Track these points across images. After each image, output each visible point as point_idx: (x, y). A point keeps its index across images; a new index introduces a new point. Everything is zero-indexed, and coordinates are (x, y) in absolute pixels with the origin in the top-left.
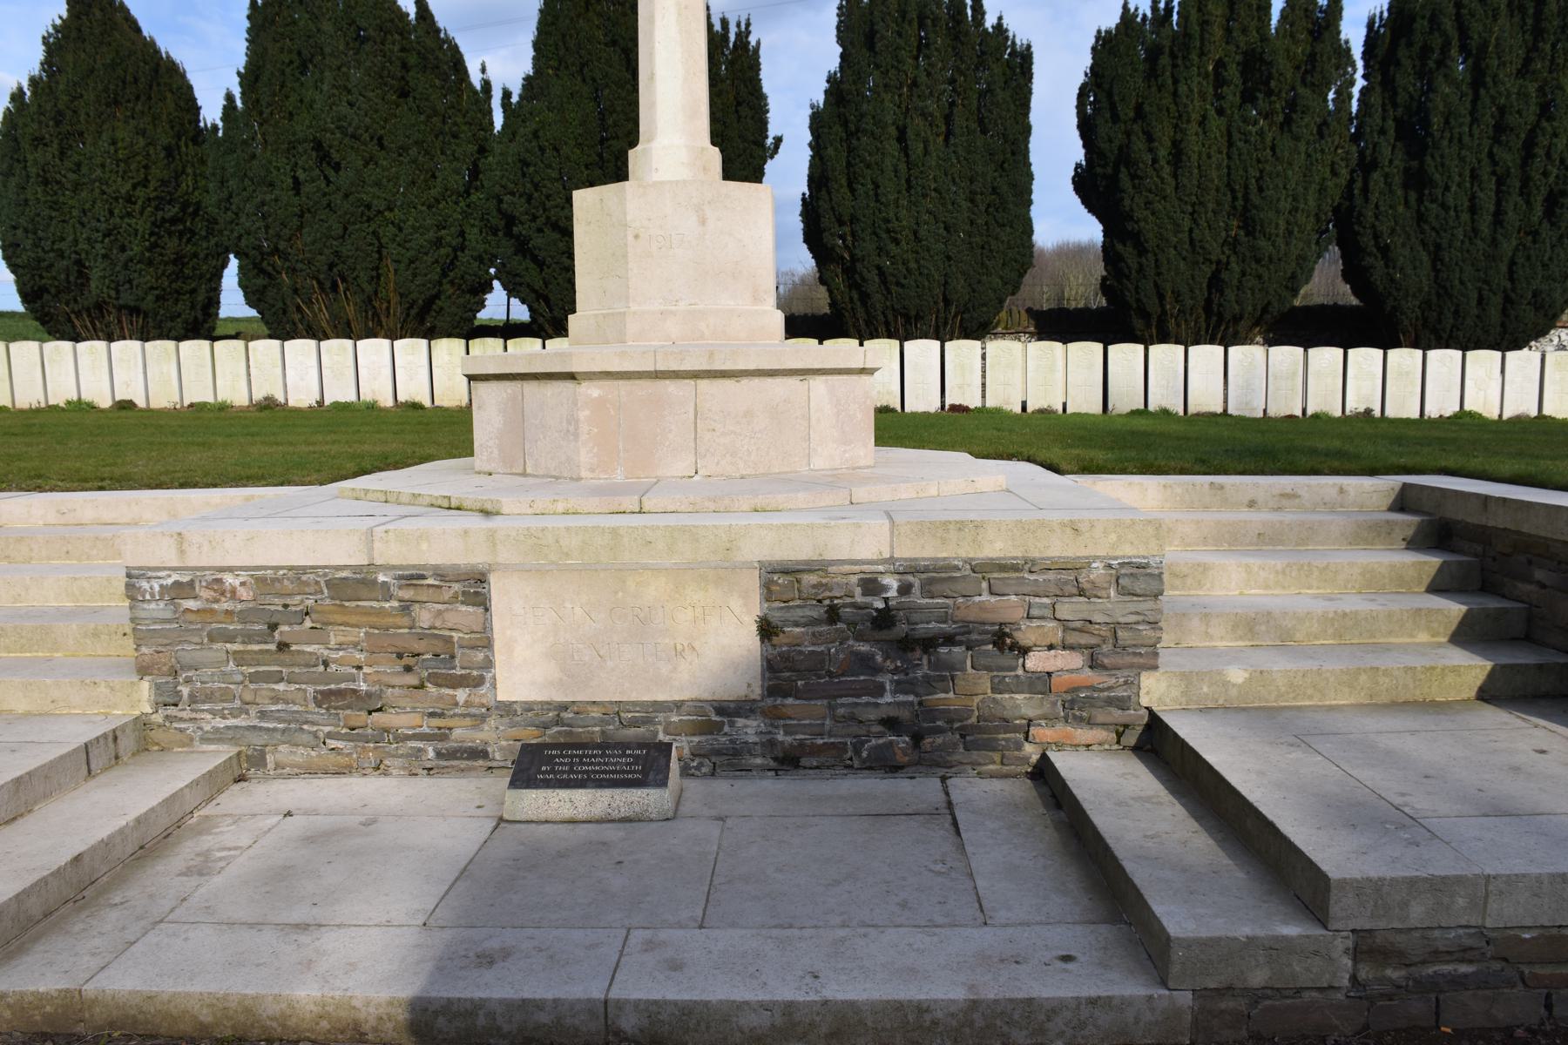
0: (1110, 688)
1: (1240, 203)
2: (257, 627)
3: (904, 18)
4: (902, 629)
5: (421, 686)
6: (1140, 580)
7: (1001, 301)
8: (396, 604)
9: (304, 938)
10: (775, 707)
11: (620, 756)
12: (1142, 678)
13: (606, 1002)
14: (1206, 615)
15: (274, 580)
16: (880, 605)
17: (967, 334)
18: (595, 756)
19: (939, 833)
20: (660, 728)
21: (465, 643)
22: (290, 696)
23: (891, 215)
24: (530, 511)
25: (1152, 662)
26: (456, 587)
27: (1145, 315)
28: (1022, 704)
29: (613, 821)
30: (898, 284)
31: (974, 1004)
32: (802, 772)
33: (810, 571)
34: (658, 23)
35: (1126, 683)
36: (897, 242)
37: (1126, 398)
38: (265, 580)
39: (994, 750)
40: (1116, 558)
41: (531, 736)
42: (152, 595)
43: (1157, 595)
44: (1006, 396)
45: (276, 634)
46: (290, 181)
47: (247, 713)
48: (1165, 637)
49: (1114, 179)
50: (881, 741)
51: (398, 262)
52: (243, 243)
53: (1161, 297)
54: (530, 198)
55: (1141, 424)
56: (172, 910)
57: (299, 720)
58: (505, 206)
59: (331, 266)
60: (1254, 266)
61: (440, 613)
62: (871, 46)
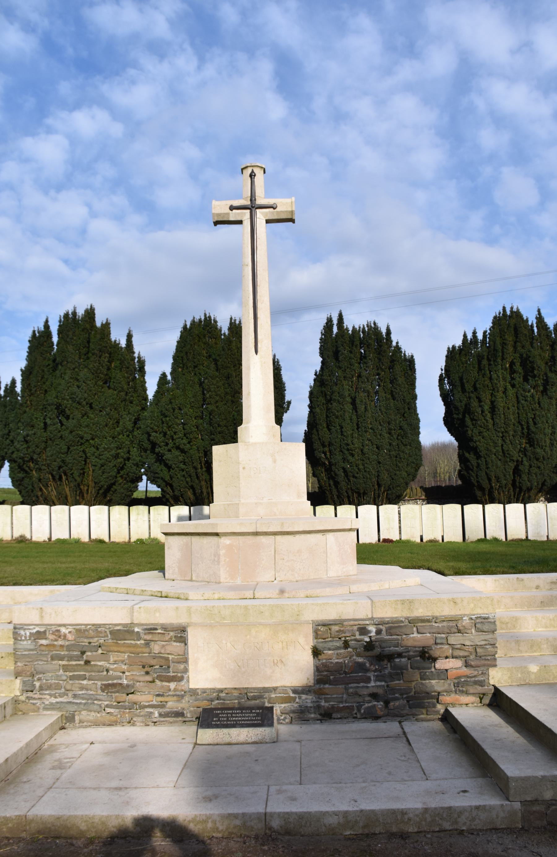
0: (475, 676)
1: (525, 431)
2: (75, 653)
3: (353, 345)
4: (377, 651)
5: (153, 681)
6: (485, 624)
7: (407, 484)
8: (143, 642)
9: (121, 793)
10: (320, 689)
11: (249, 713)
12: (490, 671)
13: (265, 814)
14: (518, 641)
15: (85, 631)
16: (367, 639)
17: (391, 501)
18: (238, 713)
19: (401, 745)
20: (266, 700)
21: (175, 660)
22: (89, 687)
23: (349, 441)
24: (202, 598)
25: (493, 663)
26: (172, 634)
27: (482, 489)
28: (436, 685)
29: (249, 743)
30: (354, 476)
31: (426, 810)
32: (333, 721)
33: (335, 624)
34: (252, 370)
35: (482, 673)
36: (353, 455)
37: (475, 532)
38: (81, 631)
39: (423, 708)
40: (474, 615)
41: (205, 704)
42: (26, 637)
43: (493, 632)
44: (411, 534)
45: (85, 656)
46: (42, 424)
47: (67, 695)
48: (499, 651)
49: (463, 420)
50: (370, 705)
51: (95, 466)
52: (14, 456)
53: (490, 480)
54: (165, 434)
55: (483, 547)
56: (54, 783)
57: (94, 698)
58: (151, 438)
59: (60, 467)
60: (535, 462)
61: (163, 646)
62: (337, 359)
